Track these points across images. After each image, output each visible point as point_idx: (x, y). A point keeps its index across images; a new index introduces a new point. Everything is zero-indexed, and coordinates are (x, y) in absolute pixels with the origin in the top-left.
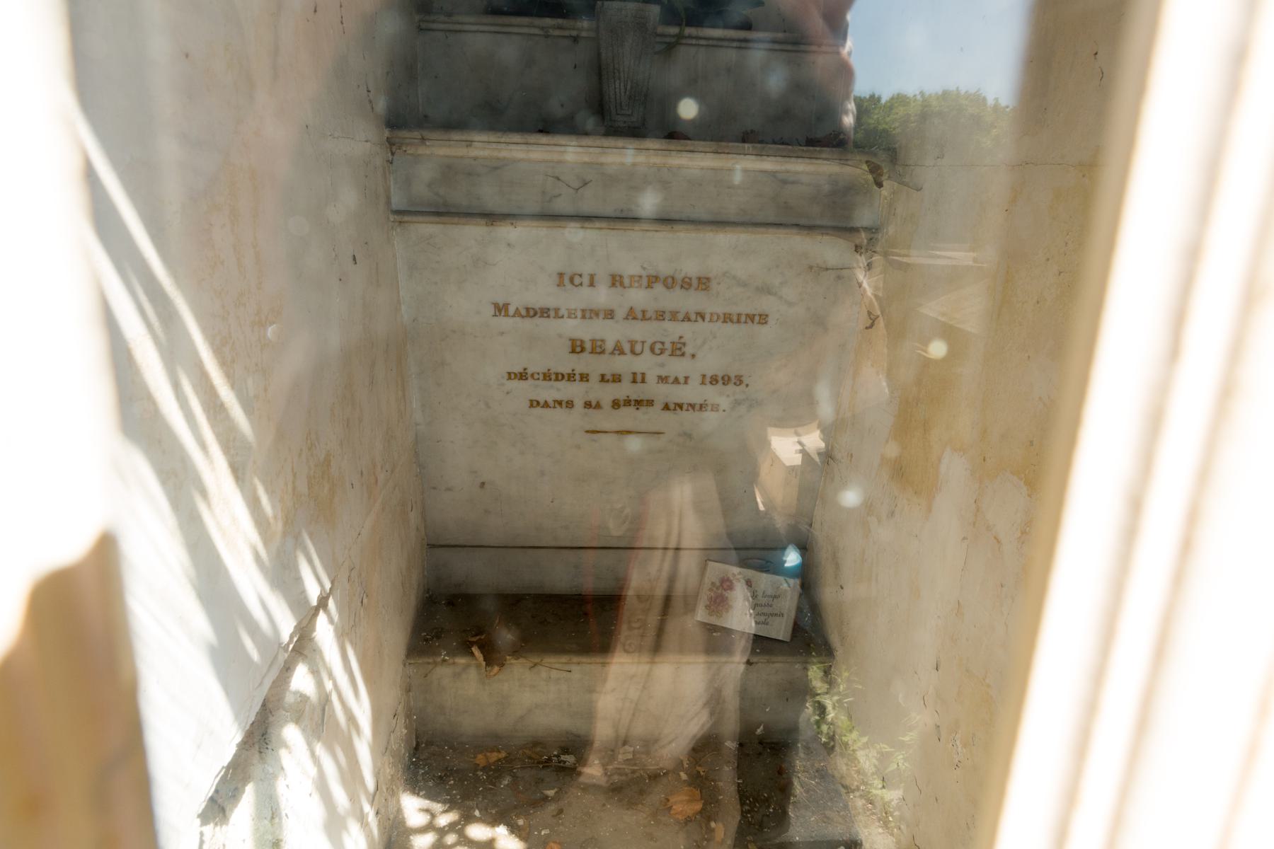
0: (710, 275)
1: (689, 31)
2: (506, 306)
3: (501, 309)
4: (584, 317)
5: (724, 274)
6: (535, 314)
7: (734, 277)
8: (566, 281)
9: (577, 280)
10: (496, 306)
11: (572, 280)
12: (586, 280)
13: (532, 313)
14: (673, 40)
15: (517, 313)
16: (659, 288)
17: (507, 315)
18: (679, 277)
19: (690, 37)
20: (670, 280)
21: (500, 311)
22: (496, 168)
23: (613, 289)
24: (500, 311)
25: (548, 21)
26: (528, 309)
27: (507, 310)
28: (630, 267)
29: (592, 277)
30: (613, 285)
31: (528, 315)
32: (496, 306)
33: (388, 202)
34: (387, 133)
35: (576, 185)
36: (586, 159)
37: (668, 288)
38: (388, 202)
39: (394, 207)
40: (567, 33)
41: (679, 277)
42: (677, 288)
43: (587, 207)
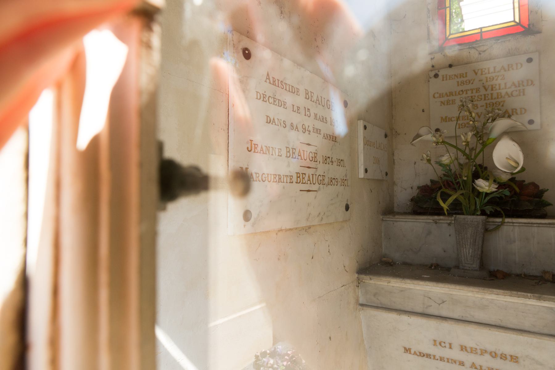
0: (518, 355)
1: (507, 220)
2: (410, 349)
3: (407, 350)
4: (448, 362)
5: (527, 356)
6: (424, 356)
7: (533, 359)
8: (438, 344)
9: (443, 344)
10: (405, 348)
11: (440, 344)
12: (448, 346)
13: (422, 355)
14: (500, 224)
15: (415, 353)
16: (487, 357)
17: (410, 353)
18: (499, 353)
19: (508, 222)
20: (493, 354)
21: (407, 351)
22: (402, 291)
23: (462, 352)
24: (407, 351)
25: (436, 217)
26: (420, 353)
27: (410, 351)
28: (470, 344)
29: (450, 344)
30: (462, 350)
31: (420, 355)
32: (405, 348)
33: (357, 300)
34: (357, 275)
35: (440, 302)
36: (443, 292)
37: (495, 357)
38: (357, 300)
39: (361, 302)
40: (445, 222)
41: (499, 353)
42: (499, 358)
43: (444, 313)
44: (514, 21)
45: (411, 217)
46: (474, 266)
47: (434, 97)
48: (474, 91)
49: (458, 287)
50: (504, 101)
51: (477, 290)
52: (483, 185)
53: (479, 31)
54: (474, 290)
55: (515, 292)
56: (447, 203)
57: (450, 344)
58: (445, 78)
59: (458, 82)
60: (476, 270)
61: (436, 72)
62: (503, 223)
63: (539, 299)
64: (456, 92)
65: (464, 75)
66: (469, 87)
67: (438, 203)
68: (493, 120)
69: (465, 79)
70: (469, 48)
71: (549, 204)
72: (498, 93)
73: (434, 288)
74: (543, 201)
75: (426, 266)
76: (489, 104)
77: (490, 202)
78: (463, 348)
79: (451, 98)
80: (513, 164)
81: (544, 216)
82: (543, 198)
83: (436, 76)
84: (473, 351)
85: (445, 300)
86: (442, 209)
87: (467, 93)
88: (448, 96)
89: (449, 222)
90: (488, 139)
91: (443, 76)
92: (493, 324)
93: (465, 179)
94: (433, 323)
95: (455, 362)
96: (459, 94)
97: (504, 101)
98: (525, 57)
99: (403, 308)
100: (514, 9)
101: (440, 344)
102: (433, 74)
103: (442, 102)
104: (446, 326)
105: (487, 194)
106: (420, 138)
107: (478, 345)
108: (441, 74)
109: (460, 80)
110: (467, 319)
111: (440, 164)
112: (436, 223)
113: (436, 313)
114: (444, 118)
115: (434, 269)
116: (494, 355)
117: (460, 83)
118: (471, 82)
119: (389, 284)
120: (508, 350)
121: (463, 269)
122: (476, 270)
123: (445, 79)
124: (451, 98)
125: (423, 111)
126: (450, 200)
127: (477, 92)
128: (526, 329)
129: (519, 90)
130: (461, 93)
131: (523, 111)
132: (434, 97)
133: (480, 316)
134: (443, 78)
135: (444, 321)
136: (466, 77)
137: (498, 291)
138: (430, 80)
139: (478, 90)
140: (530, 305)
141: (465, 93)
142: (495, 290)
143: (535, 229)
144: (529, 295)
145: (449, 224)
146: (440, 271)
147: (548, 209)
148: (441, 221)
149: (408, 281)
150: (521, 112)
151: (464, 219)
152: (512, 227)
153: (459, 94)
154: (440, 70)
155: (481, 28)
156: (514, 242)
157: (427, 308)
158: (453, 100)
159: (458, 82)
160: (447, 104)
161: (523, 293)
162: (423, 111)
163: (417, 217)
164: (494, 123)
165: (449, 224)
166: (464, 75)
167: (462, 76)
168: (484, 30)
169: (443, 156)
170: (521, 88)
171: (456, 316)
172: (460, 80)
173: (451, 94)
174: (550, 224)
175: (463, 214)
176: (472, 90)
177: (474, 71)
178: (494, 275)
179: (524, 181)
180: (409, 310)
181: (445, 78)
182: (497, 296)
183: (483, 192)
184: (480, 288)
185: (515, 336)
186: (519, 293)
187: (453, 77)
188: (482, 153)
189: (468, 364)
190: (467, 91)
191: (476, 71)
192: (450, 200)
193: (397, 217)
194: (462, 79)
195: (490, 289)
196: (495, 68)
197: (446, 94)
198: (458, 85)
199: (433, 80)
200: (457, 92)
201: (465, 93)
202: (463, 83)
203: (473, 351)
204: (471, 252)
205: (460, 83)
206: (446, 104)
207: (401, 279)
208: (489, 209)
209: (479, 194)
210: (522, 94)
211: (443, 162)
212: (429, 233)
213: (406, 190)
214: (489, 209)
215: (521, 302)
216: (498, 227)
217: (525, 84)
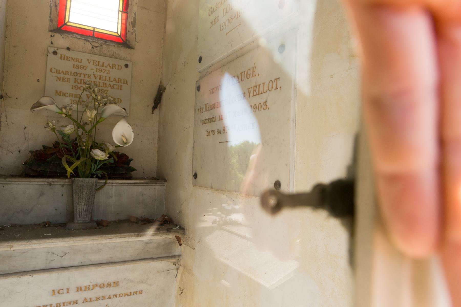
1: (109, 181)
7: (128, 280)
11: (59, 292)
19: (110, 183)
22: (24, 253)
23: (77, 293)
25: (51, 180)
36: (66, 245)
43: (65, 264)
44: (68, 22)
45: (24, 180)
46: (87, 219)
47: (51, 71)
48: (86, 76)
49: (81, 238)
50: (108, 91)
51: (97, 238)
52: (100, 155)
53: (92, 29)
54: (95, 238)
55: (123, 234)
56: (71, 167)
57: (68, 289)
58: (63, 57)
59: (74, 65)
60: (88, 222)
61: (56, 49)
62: (105, 184)
63: (138, 236)
64: (71, 72)
65: (80, 61)
66: (82, 71)
67: (64, 168)
68: (105, 104)
69: (80, 64)
70: (85, 40)
71: (134, 170)
72: (104, 83)
73: (59, 243)
74: (131, 167)
75: (39, 225)
76: (75, 87)
77: (101, 168)
78: (79, 289)
79: (67, 76)
80: (125, 141)
81: (130, 178)
82: (131, 165)
83: (55, 53)
84: (87, 288)
85: (67, 252)
86: (66, 171)
87: (80, 76)
88: (64, 74)
89: (62, 183)
90: (101, 118)
91: (61, 55)
92: (105, 262)
93: (84, 148)
94: (54, 275)
95: (70, 303)
96: (74, 75)
97: (108, 91)
98: (123, 63)
99: (23, 270)
100: (118, 23)
101: (59, 292)
102: (51, 50)
103: (58, 77)
104: (66, 274)
105: (100, 161)
106: (44, 107)
107: (91, 283)
108: (59, 52)
109: (76, 63)
110: (86, 264)
111: (62, 133)
112: (50, 185)
113: (59, 265)
114: (58, 92)
115: (48, 227)
116: (101, 286)
117: (75, 66)
118: (85, 68)
119: (12, 249)
120: (112, 279)
121: (77, 223)
122: (88, 222)
123: (63, 58)
124: (67, 76)
125: (38, 81)
126: (74, 166)
127: (88, 78)
128: (127, 260)
129: (118, 85)
130: (75, 74)
131: (120, 101)
132: (51, 71)
133: (96, 258)
134: (61, 57)
135: (66, 271)
136: (81, 62)
137: (112, 235)
138: (49, 54)
139: (89, 76)
140: (130, 241)
141: (79, 75)
142: (110, 235)
143: (125, 188)
144: (132, 234)
145: (63, 186)
146: (60, 226)
147: (133, 173)
148: (55, 183)
149: (34, 242)
150: (118, 101)
151: (82, 181)
152: (111, 187)
153: (74, 75)
154: (59, 49)
155: (94, 28)
156: (112, 197)
157: (49, 263)
158: (68, 79)
159: (74, 65)
160: (63, 81)
161: (128, 234)
162: (38, 81)
163: (32, 180)
164: (106, 107)
165: (63, 186)
166: (80, 61)
167: (77, 60)
168: (96, 30)
169: (66, 126)
170: (120, 84)
171: (76, 263)
172: (76, 63)
173: (67, 73)
174: (135, 183)
175: (79, 177)
176: (85, 75)
177: (88, 60)
178: (100, 226)
179: (119, 152)
180: (31, 270)
181: (63, 57)
182: (111, 240)
183: (97, 160)
184: (99, 236)
185: (119, 267)
186: (126, 234)
187: (70, 59)
188: (94, 129)
189: (80, 301)
190: (80, 74)
191: (90, 61)
192: (74, 166)
193: (8, 179)
194: (77, 63)
195: (107, 236)
196: (103, 63)
197: (63, 71)
198: (74, 68)
199: (51, 56)
200: (72, 73)
201: (79, 75)
202: (78, 67)
203: (87, 288)
204: (85, 208)
205: (75, 66)
206: (61, 80)
207: (26, 241)
208: (100, 173)
209: (95, 161)
210: (120, 88)
211: (65, 132)
212: (42, 194)
213: (12, 153)
214: (100, 173)
215: (126, 240)
216: (102, 187)
217: (122, 81)
